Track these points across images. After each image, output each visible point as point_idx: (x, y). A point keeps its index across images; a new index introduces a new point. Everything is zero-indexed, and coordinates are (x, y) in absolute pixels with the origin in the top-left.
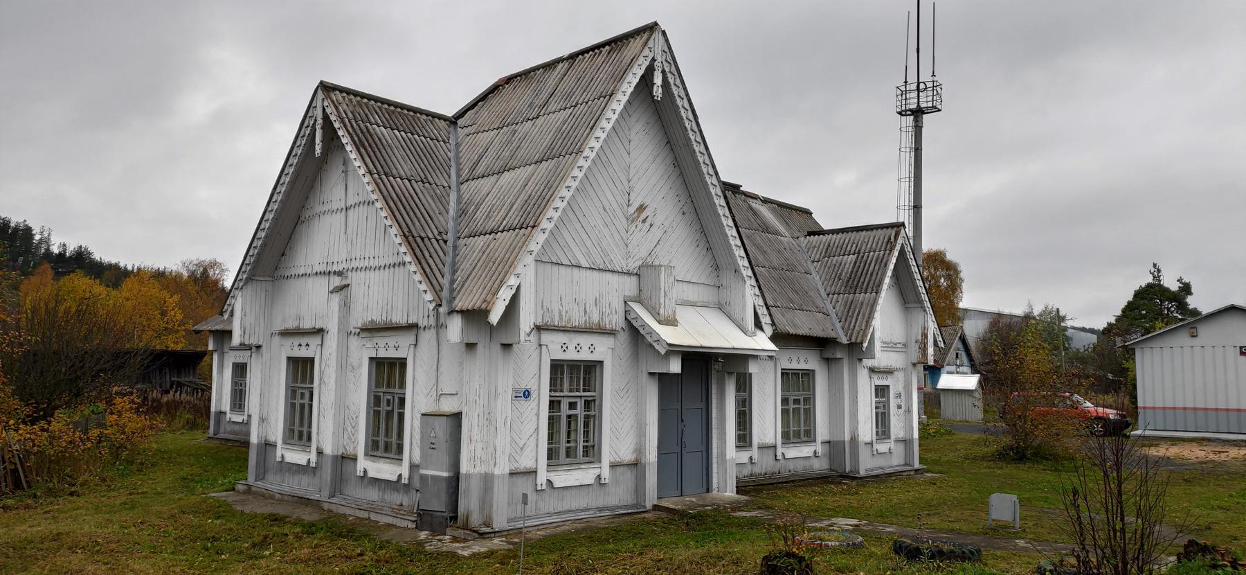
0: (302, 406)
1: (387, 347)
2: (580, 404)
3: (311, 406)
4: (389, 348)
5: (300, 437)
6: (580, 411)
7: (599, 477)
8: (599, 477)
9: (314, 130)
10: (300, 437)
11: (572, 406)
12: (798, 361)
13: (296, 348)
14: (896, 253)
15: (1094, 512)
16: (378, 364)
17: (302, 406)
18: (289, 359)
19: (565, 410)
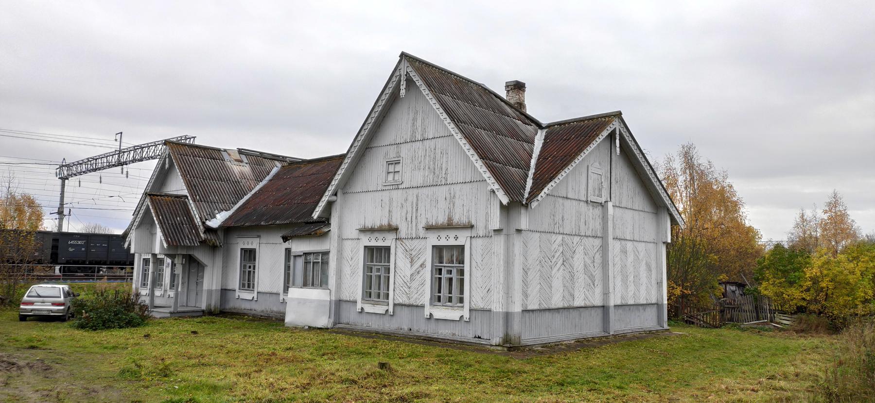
0: (249, 272)
1: (248, 243)
2: (454, 271)
3: (462, 281)
4: (447, 239)
5: (249, 287)
6: (454, 275)
7: (387, 311)
8: (387, 311)
9: (400, 81)
10: (249, 287)
11: (450, 272)
12: (377, 239)
13: (373, 240)
14: (618, 142)
15: (193, 295)
16: (370, 251)
17: (249, 272)
18: (365, 247)
19: (445, 275)
